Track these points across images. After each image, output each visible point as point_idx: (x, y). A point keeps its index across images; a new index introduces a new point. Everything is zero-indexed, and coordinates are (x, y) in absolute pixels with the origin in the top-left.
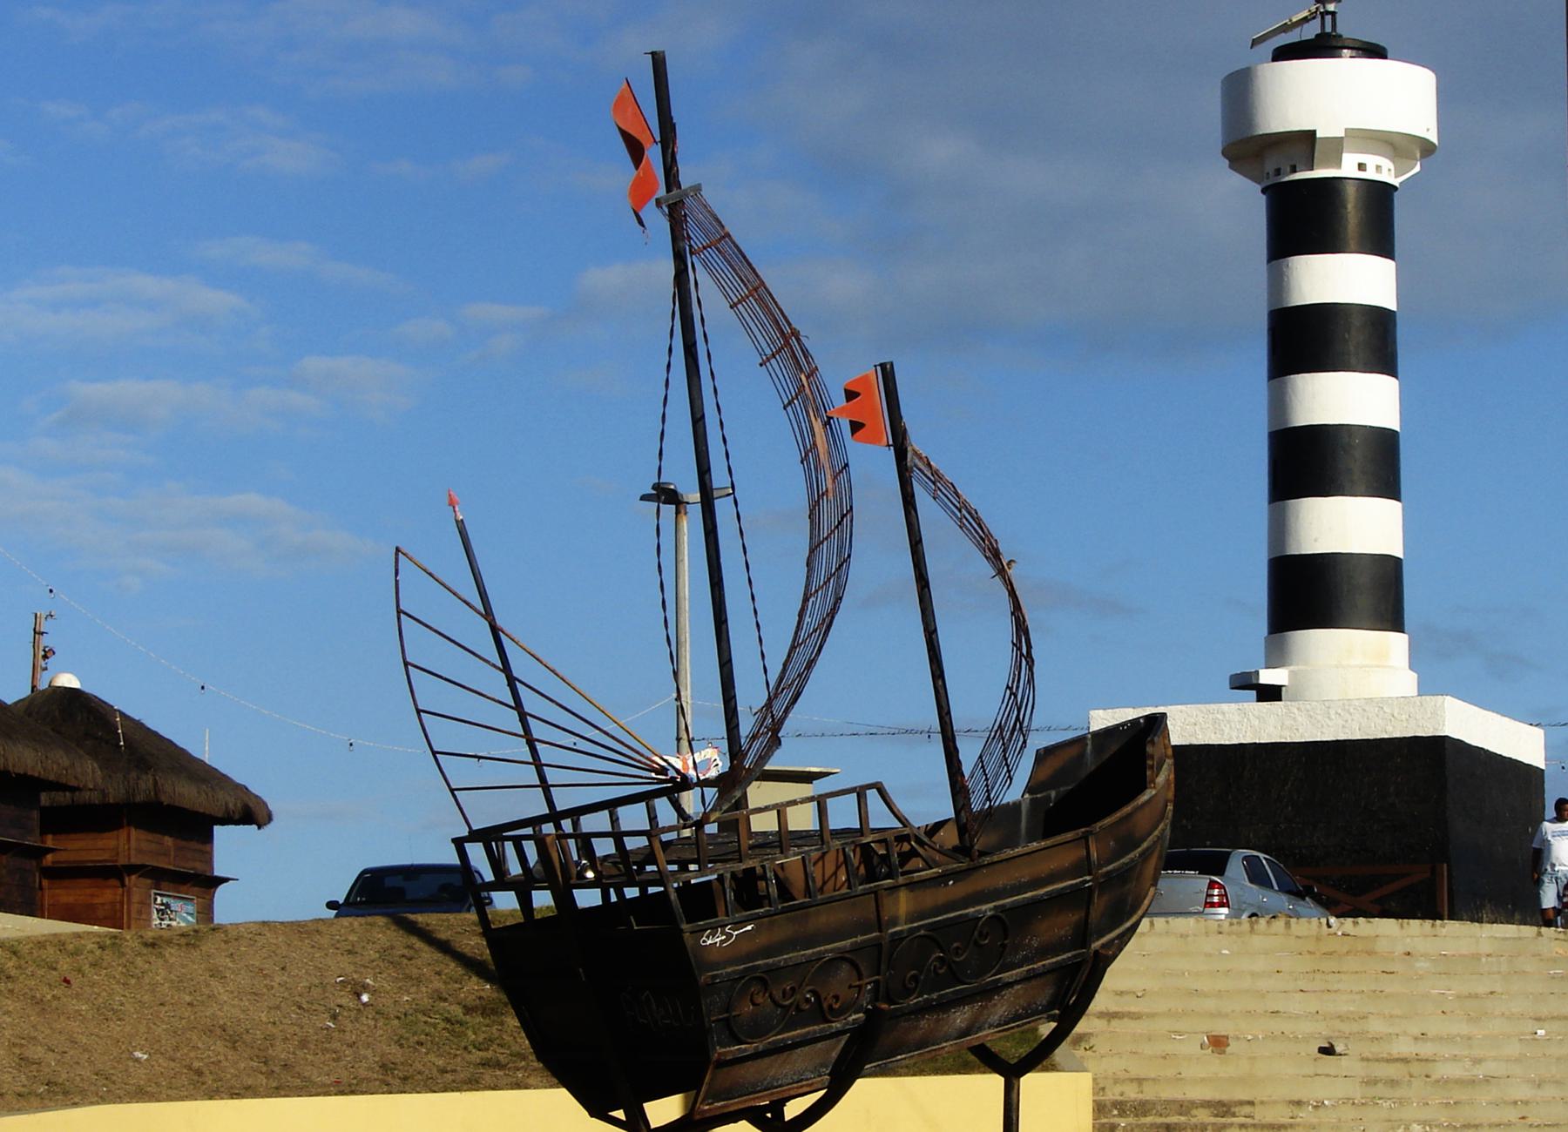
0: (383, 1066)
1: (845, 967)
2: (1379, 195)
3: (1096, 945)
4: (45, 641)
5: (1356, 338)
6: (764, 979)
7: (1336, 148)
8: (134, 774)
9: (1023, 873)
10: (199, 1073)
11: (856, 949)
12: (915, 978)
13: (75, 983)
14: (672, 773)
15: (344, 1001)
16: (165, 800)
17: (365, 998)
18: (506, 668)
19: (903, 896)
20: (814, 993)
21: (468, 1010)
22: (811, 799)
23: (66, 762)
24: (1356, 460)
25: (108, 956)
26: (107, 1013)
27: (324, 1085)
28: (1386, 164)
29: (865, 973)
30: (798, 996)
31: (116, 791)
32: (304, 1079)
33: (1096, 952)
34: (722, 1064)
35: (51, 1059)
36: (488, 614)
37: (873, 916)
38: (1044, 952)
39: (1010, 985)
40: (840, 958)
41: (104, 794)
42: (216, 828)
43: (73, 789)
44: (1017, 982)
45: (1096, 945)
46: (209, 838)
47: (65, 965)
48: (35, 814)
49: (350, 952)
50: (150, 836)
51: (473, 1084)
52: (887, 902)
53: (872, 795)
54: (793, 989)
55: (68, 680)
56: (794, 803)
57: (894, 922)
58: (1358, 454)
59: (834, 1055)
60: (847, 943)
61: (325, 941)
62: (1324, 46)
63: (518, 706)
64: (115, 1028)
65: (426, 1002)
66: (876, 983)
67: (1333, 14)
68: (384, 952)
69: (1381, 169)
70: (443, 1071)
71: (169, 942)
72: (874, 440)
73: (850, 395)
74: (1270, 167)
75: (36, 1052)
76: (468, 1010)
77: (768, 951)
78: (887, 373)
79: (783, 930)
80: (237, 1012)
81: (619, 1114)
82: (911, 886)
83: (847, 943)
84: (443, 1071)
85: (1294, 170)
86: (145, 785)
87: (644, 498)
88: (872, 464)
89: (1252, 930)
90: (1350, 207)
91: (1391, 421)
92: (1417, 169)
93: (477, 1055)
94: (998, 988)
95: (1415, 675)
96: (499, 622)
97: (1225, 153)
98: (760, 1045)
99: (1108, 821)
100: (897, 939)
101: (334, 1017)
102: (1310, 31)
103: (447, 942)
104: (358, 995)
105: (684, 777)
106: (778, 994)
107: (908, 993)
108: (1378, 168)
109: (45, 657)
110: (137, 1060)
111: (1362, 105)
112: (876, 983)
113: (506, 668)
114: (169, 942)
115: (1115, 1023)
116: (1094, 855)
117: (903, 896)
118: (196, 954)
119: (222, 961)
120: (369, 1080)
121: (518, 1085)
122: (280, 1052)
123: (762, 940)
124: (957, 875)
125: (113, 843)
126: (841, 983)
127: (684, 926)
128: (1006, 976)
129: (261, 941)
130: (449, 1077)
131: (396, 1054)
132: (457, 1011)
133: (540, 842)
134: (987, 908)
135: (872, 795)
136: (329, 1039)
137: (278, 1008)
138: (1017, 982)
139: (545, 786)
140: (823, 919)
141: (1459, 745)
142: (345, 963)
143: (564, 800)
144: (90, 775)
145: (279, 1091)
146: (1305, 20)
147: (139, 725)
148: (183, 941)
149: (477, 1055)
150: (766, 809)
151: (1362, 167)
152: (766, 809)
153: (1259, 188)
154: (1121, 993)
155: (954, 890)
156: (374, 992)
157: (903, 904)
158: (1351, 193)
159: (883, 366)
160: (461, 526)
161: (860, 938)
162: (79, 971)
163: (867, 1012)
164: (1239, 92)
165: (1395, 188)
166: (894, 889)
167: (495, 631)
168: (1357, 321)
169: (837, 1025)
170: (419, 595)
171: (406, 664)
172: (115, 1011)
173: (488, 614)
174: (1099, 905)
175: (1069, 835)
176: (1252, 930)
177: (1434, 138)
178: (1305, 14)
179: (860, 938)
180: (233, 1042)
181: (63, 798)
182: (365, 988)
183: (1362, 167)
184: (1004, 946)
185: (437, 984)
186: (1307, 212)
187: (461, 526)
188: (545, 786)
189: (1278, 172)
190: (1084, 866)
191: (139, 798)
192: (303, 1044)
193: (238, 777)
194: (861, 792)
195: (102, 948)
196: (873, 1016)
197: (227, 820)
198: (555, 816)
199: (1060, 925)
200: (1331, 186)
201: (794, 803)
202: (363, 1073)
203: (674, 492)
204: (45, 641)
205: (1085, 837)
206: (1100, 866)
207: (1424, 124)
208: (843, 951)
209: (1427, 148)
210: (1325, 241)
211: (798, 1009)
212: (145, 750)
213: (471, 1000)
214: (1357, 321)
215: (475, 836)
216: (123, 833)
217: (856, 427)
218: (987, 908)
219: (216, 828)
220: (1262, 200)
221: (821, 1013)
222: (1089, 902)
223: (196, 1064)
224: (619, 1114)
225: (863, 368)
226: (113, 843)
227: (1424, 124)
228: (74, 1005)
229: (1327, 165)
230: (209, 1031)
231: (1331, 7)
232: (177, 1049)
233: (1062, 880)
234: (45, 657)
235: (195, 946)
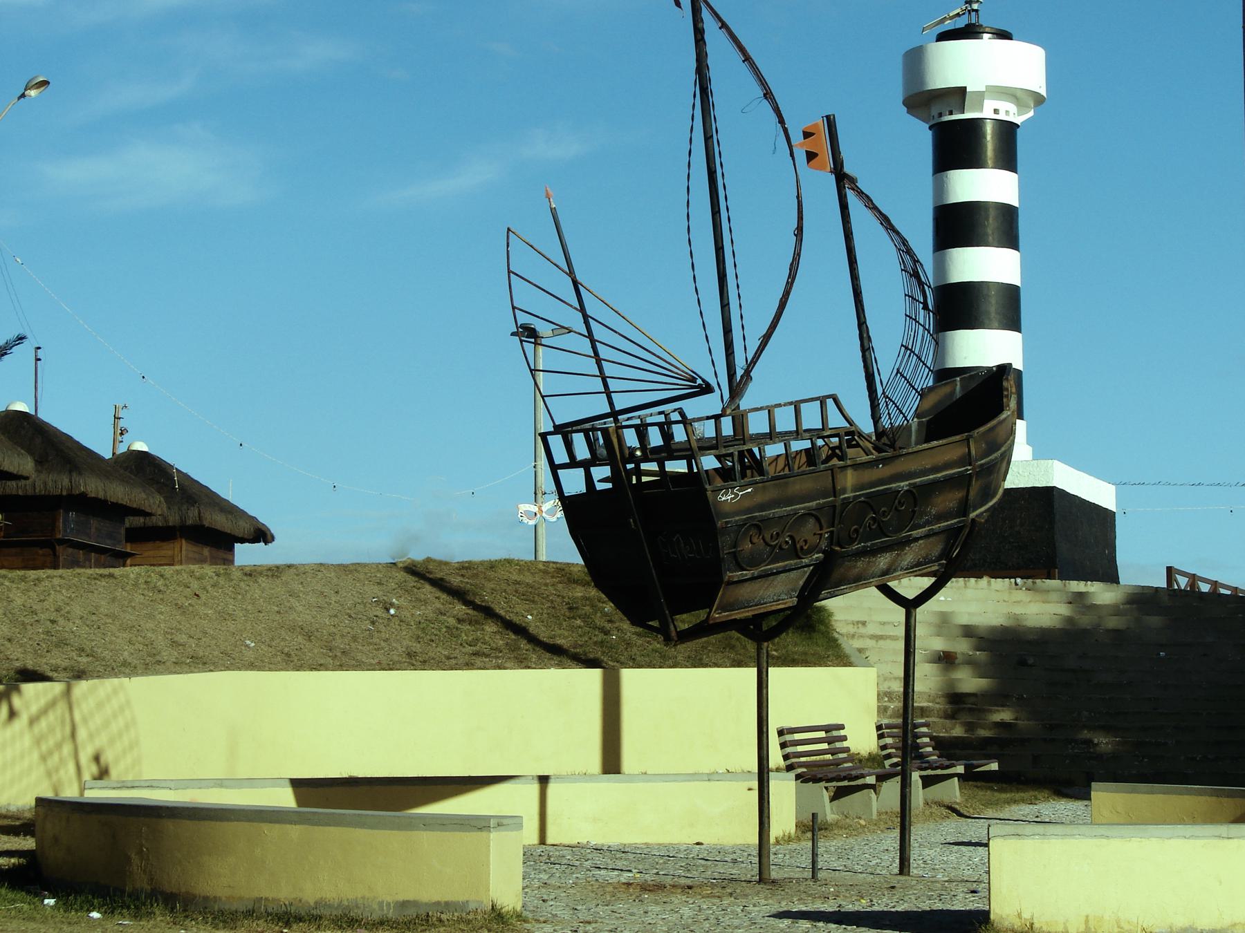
0: (409, 654)
1: (812, 521)
2: (1007, 131)
3: (973, 515)
4: (122, 423)
5: (992, 225)
6: (759, 526)
7: (980, 96)
8: (185, 507)
9: (927, 463)
10: (288, 655)
11: (820, 508)
12: (856, 531)
13: (203, 597)
14: (699, 381)
15: (379, 613)
16: (207, 524)
17: (392, 611)
18: (582, 309)
19: (850, 472)
20: (791, 537)
21: (459, 621)
22: (791, 403)
23: (144, 496)
24: (993, 305)
25: (222, 581)
26: (224, 616)
27: (371, 664)
28: (1012, 108)
29: (825, 525)
30: (781, 539)
31: (174, 519)
32: (357, 661)
33: (973, 520)
34: (730, 583)
35: (193, 643)
36: (571, 273)
37: (830, 485)
38: (940, 517)
39: (916, 540)
40: (809, 514)
41: (166, 520)
42: (237, 545)
43: (150, 515)
44: (921, 538)
45: (973, 515)
46: (231, 549)
47: (195, 585)
48: (123, 531)
49: (379, 584)
50: (195, 549)
51: (469, 666)
52: (839, 477)
53: (830, 402)
54: (778, 534)
55: (140, 446)
56: (779, 405)
57: (844, 491)
58: (993, 301)
59: (801, 583)
60: (813, 504)
61: (362, 576)
62: (970, 32)
63: (590, 335)
64: (232, 626)
65: (432, 616)
66: (832, 532)
67: (977, 11)
68: (400, 585)
69: (1009, 111)
70: (449, 658)
71: (261, 574)
72: (821, 168)
73: (807, 135)
74: (934, 112)
75: (182, 638)
76: (459, 621)
77: (762, 507)
78: (831, 122)
79: (771, 494)
80: (309, 618)
81: (655, 623)
82: (857, 466)
83: (813, 504)
84: (449, 658)
85: (951, 113)
86: (192, 516)
87: (513, 334)
88: (821, 184)
89: (966, 586)
90: (989, 137)
91: (1016, 280)
92: (1031, 113)
93: (469, 649)
94: (909, 541)
95: (1030, 448)
96: (579, 278)
97: (905, 103)
98: (756, 572)
99: (982, 429)
100: (846, 502)
101: (373, 623)
102: (961, 23)
103: (442, 579)
104: (388, 610)
105: (708, 384)
106: (768, 538)
107: (852, 541)
108: (1007, 112)
109: (122, 434)
110: (247, 646)
111: (995, 72)
112: (832, 532)
113: (582, 309)
114: (261, 574)
115: (881, 642)
116: (973, 452)
117: (850, 472)
118: (278, 581)
119: (297, 587)
120: (400, 662)
121: (499, 667)
122: (339, 643)
123: (759, 499)
124: (885, 461)
125: (170, 553)
126: (808, 532)
127: (707, 487)
128: (915, 533)
129: (320, 575)
130: (453, 662)
131: (417, 647)
132: (452, 621)
133: (605, 432)
134: (904, 485)
135: (830, 402)
136: (371, 636)
137: (336, 616)
138: (921, 538)
139: (608, 393)
140: (797, 487)
141: (1063, 493)
142: (376, 589)
143: (621, 402)
144: (155, 504)
145: (341, 667)
146: (958, 15)
147: (186, 476)
148: (270, 573)
149: (469, 649)
150: (761, 409)
151: (996, 111)
152: (761, 409)
153: (927, 126)
154: (884, 624)
155: (882, 471)
156: (398, 608)
157: (849, 479)
158: (989, 129)
159: (828, 117)
160: (554, 212)
161: (821, 501)
162: (204, 588)
163: (824, 552)
164: (915, 61)
165: (1018, 126)
166: (844, 468)
167: (576, 284)
168: (992, 213)
169: (805, 561)
170: (524, 261)
171: (514, 308)
172: (230, 615)
173: (571, 273)
174: (976, 486)
175: (958, 438)
176: (966, 586)
177: (1043, 92)
178: (958, 11)
179: (821, 501)
180: (309, 637)
181: (139, 521)
182: (392, 605)
183: (996, 111)
184: (914, 512)
185: (438, 605)
186: (957, 144)
187: (554, 212)
188: (608, 393)
189: (940, 115)
190: (967, 459)
191: (190, 522)
192: (355, 639)
193: (251, 513)
194: (822, 401)
195: (218, 575)
196: (829, 555)
197: (242, 541)
198: (614, 414)
199: (948, 500)
200: (976, 124)
201: (779, 405)
202: (396, 658)
203: (534, 330)
204: (122, 423)
205: (967, 440)
206: (977, 460)
207: (1037, 82)
208: (808, 508)
209: (1038, 100)
210: (972, 160)
211: (781, 548)
212: (189, 493)
213: (460, 615)
214: (992, 213)
215: (559, 429)
216: (177, 545)
217: (811, 156)
218: (904, 485)
219: (237, 545)
220: (930, 133)
221: (796, 552)
222: (969, 485)
223: (286, 650)
224: (655, 623)
225: (815, 120)
226: (170, 553)
227: (1037, 82)
228: (203, 610)
229: (973, 111)
230: (292, 629)
231: (975, 6)
232: (272, 639)
233: (952, 468)
234: (122, 434)
235: (278, 577)
